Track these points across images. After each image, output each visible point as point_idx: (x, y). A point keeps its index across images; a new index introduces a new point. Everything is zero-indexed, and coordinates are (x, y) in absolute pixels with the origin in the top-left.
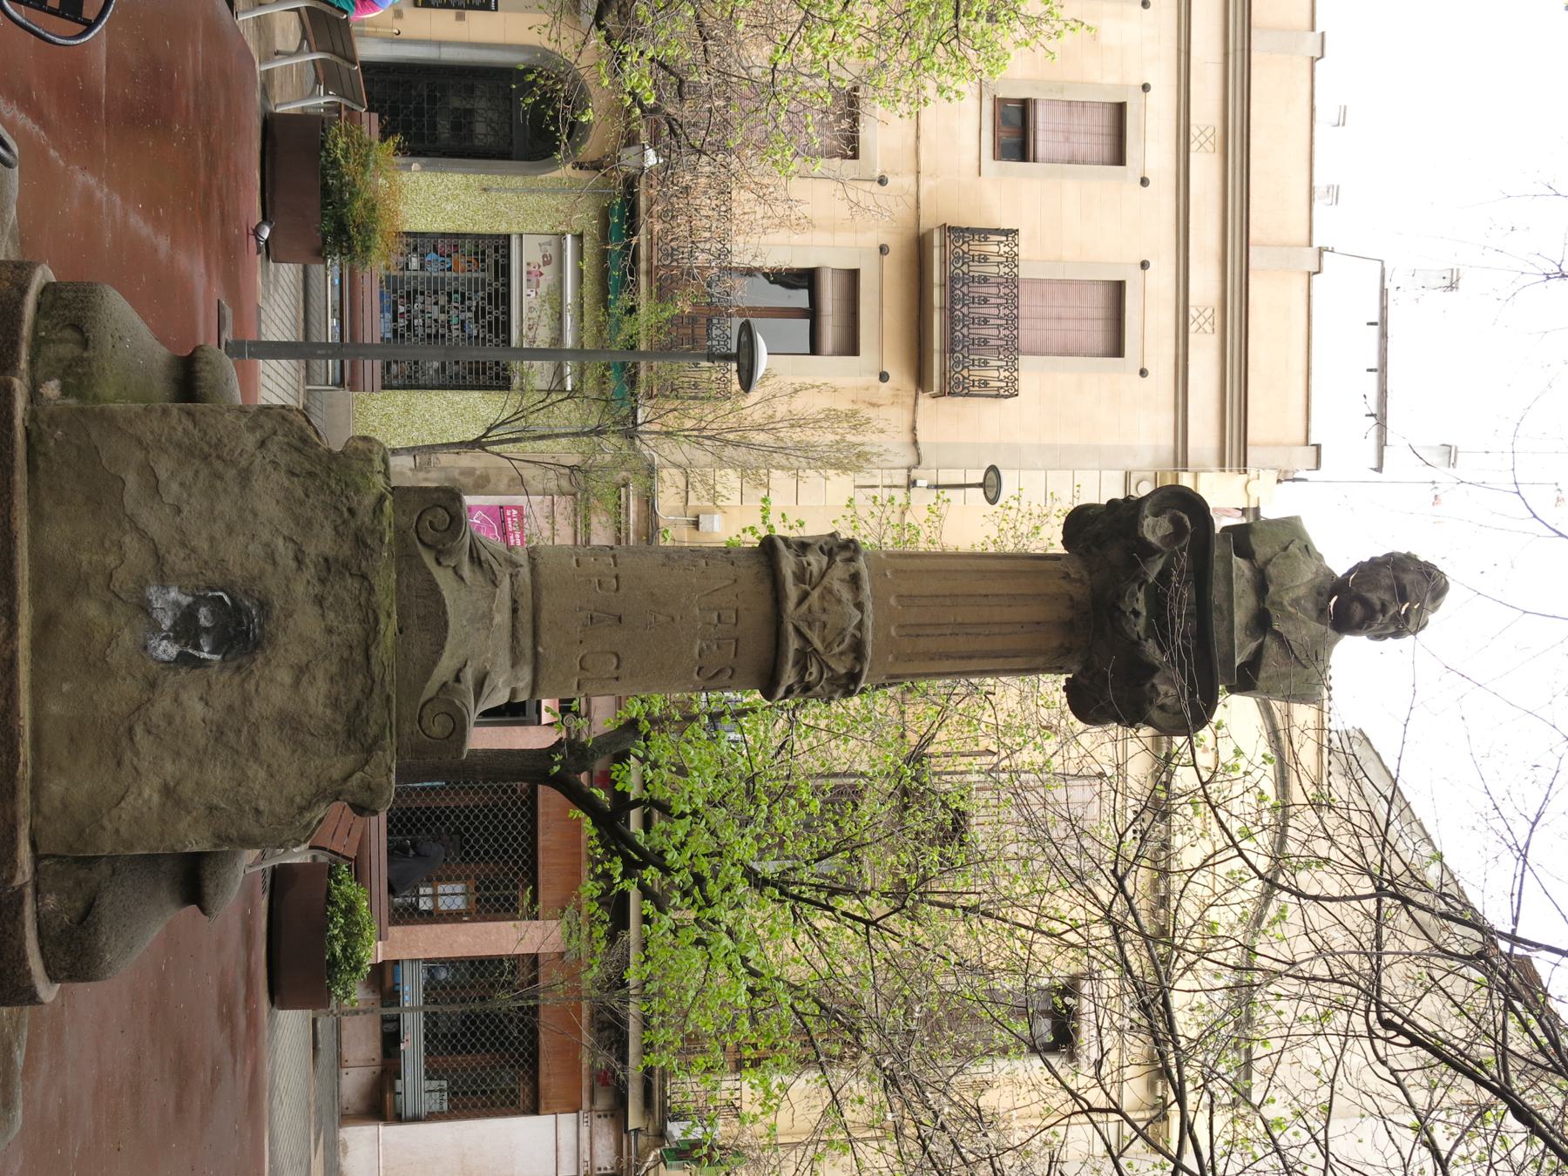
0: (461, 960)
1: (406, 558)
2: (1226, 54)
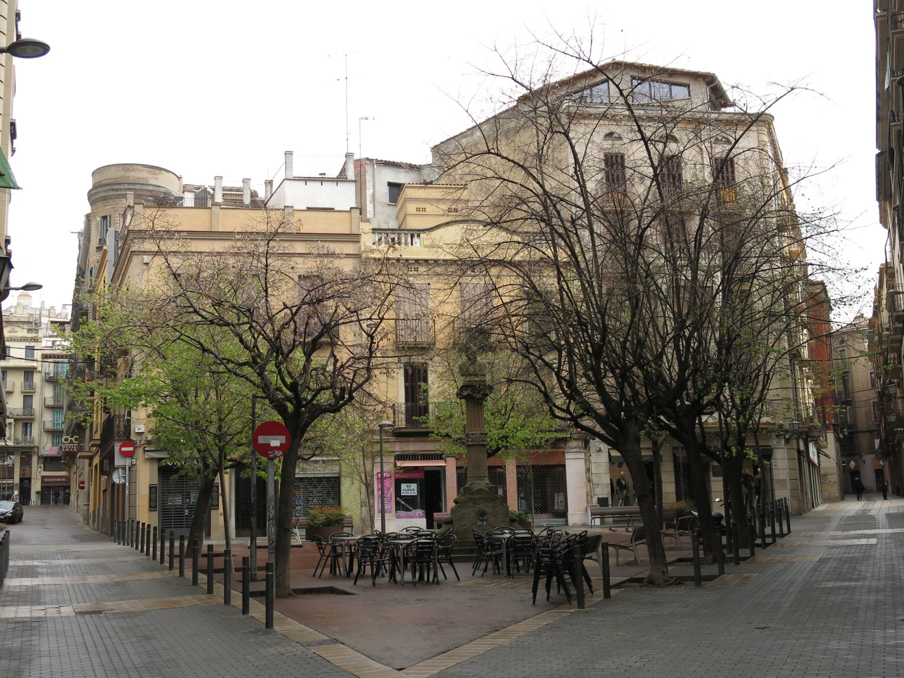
0: (518, 490)
1: (472, 494)
2: (221, 239)
